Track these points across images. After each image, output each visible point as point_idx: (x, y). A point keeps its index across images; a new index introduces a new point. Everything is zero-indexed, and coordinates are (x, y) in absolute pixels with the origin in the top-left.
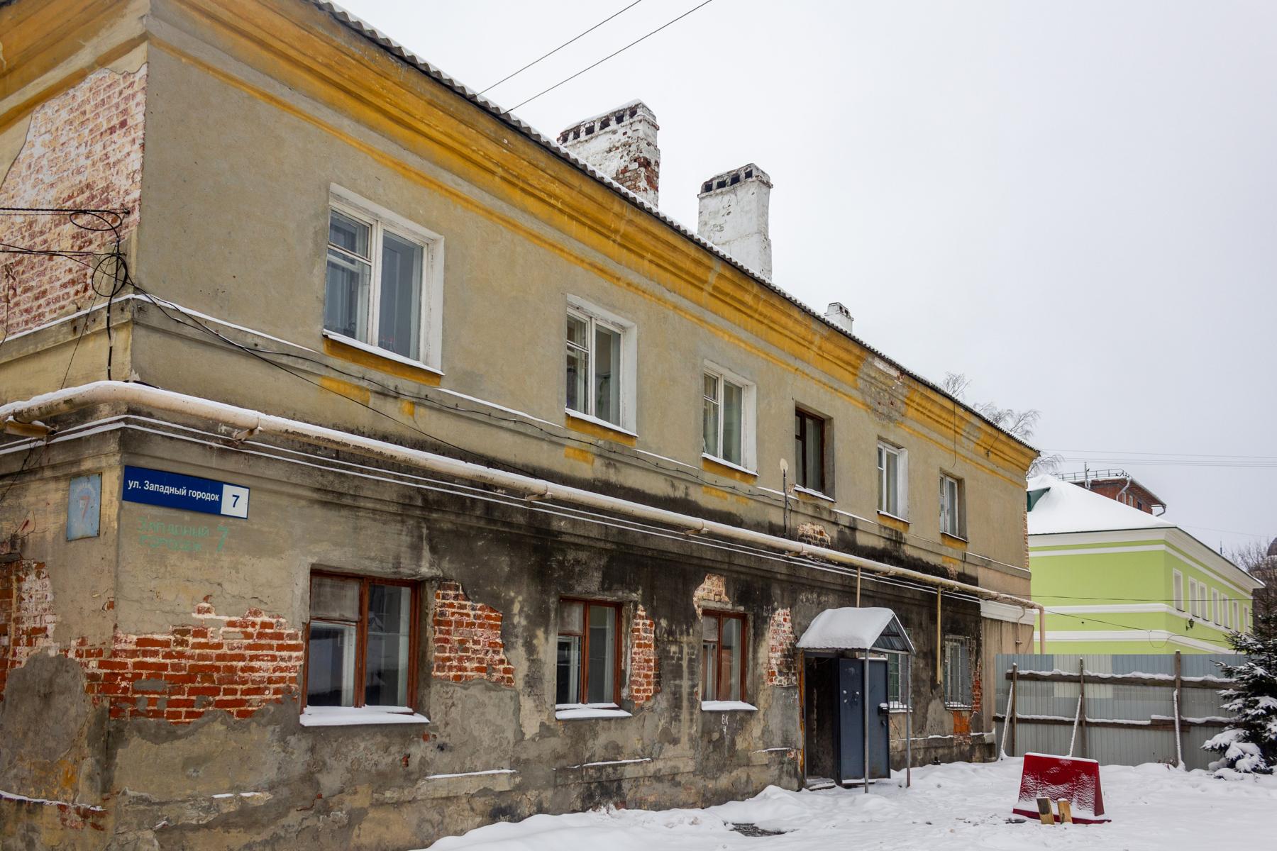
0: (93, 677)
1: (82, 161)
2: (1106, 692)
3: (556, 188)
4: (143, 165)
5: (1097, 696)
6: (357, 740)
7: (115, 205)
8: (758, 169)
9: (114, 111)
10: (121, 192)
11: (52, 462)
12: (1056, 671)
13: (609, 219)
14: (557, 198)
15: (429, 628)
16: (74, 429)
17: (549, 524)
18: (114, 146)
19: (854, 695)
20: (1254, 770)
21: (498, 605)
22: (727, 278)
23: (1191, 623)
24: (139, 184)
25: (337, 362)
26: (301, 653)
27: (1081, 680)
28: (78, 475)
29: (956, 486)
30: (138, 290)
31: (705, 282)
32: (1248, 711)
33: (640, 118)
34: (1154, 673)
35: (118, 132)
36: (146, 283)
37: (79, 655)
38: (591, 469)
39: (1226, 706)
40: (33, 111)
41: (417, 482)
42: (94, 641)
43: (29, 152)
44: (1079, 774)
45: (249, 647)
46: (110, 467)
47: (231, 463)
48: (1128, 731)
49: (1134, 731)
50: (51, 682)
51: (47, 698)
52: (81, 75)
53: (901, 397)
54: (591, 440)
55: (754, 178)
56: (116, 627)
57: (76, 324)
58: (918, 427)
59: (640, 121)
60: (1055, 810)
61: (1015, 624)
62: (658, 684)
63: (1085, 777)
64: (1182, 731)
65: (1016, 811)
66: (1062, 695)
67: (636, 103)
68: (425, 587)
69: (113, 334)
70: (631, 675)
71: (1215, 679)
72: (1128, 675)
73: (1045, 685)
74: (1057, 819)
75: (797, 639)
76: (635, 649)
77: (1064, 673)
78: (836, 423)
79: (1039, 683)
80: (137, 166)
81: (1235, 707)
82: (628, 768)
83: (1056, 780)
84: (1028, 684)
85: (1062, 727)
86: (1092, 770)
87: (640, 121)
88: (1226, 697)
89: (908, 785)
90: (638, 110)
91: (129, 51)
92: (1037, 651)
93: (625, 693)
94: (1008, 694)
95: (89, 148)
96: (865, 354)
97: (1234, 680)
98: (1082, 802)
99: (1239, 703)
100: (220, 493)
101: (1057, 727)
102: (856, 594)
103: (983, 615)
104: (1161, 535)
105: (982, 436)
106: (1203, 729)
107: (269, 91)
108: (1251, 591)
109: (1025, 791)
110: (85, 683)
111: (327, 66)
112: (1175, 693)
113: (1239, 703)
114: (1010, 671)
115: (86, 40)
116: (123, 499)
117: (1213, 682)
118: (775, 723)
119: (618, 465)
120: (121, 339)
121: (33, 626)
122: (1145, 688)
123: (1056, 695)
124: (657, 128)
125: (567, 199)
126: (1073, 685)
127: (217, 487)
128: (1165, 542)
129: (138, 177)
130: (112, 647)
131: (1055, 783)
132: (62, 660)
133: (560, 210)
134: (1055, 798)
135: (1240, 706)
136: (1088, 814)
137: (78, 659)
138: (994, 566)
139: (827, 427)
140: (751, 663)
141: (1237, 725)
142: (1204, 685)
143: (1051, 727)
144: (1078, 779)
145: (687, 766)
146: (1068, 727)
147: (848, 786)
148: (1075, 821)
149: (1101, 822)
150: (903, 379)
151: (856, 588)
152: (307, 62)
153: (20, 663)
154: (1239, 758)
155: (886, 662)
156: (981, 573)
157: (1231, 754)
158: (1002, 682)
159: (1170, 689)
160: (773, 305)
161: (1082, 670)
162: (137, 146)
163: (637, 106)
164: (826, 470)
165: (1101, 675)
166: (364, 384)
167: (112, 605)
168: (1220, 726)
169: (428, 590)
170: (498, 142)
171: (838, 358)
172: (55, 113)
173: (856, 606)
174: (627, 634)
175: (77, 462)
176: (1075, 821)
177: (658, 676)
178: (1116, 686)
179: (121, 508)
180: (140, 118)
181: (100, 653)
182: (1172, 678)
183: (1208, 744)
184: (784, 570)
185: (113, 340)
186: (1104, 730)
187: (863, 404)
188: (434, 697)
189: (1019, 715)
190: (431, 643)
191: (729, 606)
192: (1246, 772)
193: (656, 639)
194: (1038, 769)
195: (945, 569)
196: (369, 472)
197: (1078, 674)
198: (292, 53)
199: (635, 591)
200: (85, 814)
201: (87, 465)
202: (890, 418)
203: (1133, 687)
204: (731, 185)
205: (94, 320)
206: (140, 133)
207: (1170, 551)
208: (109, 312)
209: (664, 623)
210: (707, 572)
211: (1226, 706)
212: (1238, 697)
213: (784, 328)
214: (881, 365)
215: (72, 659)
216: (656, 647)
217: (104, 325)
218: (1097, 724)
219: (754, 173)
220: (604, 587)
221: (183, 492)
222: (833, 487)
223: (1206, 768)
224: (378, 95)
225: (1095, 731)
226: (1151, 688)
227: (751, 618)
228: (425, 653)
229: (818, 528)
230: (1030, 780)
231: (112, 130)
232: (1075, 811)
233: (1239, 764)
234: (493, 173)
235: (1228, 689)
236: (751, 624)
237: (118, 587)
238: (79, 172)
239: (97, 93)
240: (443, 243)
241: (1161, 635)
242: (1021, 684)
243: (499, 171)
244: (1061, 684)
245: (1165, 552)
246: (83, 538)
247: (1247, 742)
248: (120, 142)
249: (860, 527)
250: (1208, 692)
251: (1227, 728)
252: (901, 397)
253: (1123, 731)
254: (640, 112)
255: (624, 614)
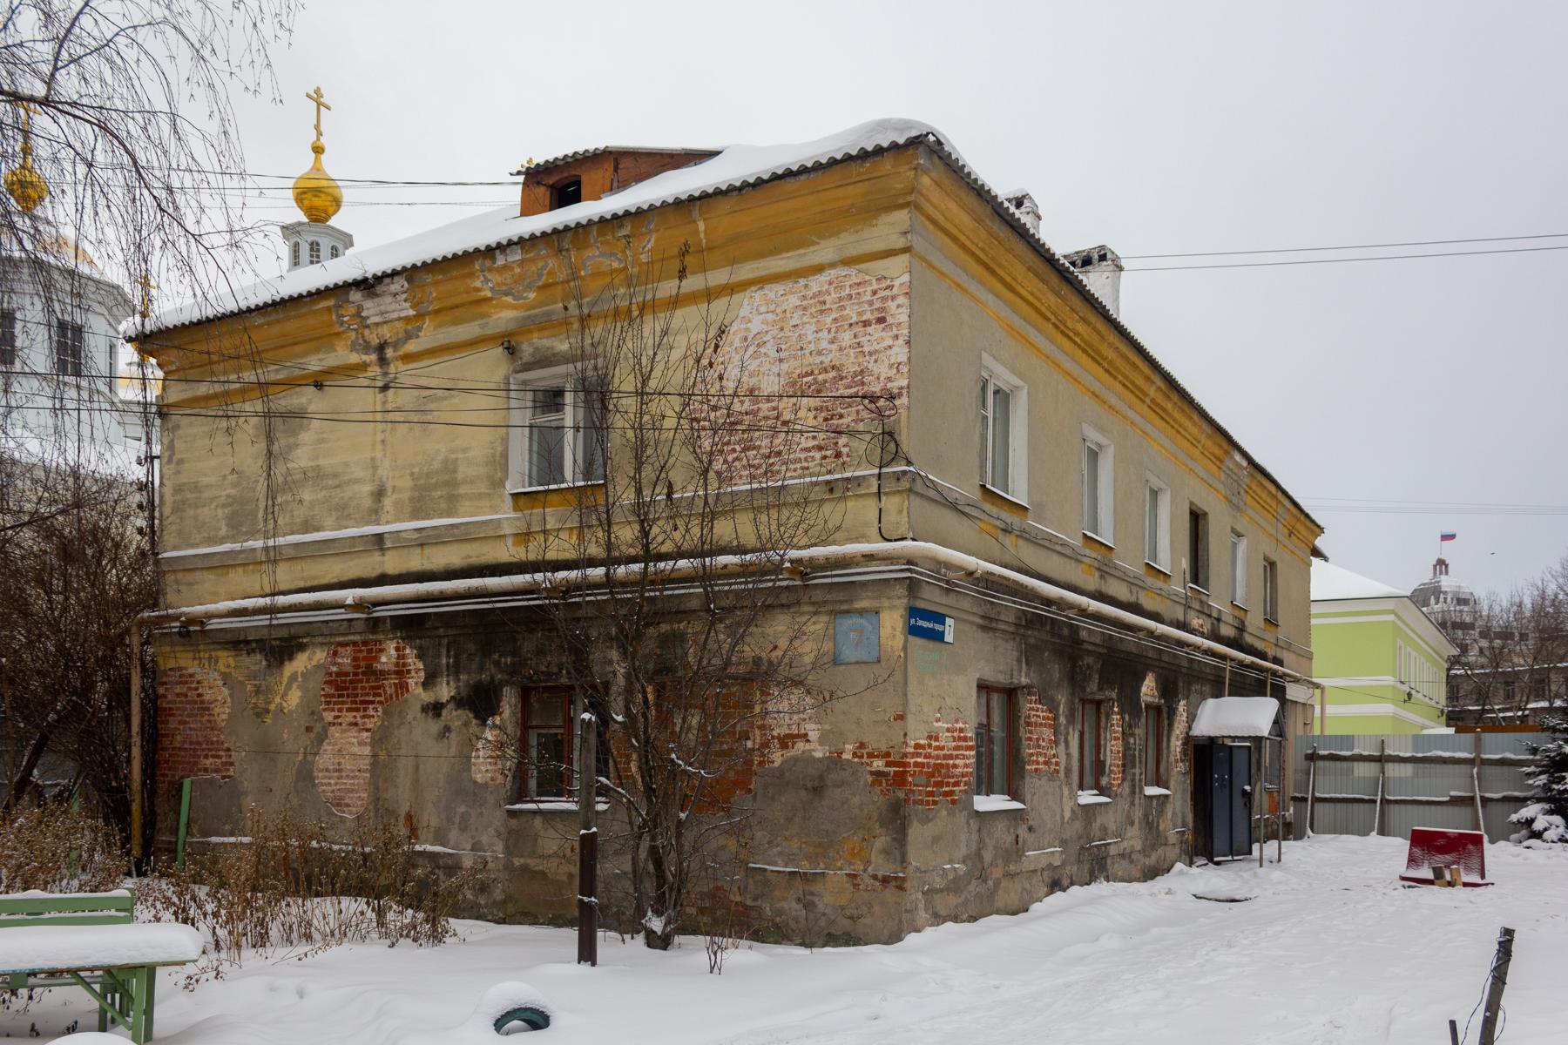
0: (878, 774)
1: (824, 344)
2: (1406, 770)
3: (1080, 327)
4: (909, 359)
5: (1397, 775)
6: (997, 822)
7: (876, 388)
8: (1113, 253)
9: (866, 307)
10: (882, 379)
11: (813, 600)
12: (1356, 751)
13: (1104, 348)
14: (1077, 334)
15: (1022, 729)
16: (834, 573)
17: (1078, 635)
18: (868, 338)
19: (1224, 779)
20: (1560, 840)
21: (1053, 708)
22: (1162, 390)
23: (1410, 695)
24: (906, 375)
25: (987, 507)
26: (973, 753)
27: (1381, 759)
28: (847, 612)
29: (1268, 569)
30: (909, 463)
31: (1146, 395)
32: (1555, 787)
33: (1028, 210)
34: (1454, 752)
35: (873, 326)
36: (913, 458)
37: (855, 755)
38: (1092, 583)
39: (1531, 782)
40: (746, 290)
41: (1021, 604)
42: (876, 742)
43: (743, 326)
44: (1466, 845)
45: (957, 748)
46: (893, 607)
47: (950, 600)
48: (1427, 808)
49: (1433, 808)
50: (821, 778)
51: (818, 790)
52: (819, 269)
53: (1245, 486)
54: (1094, 555)
55: (1110, 262)
56: (905, 735)
57: (832, 485)
58: (1256, 517)
59: (1028, 213)
60: (1448, 877)
61: (1304, 704)
62: (1124, 772)
63: (1471, 847)
64: (1483, 806)
65: (1404, 879)
66: (1362, 775)
67: (1024, 193)
68: (1016, 694)
69: (883, 498)
70: (1110, 766)
71: (1513, 756)
72: (1429, 754)
73: (1345, 764)
74: (1450, 884)
75: (1190, 728)
76: (1113, 742)
77: (1365, 753)
78: (1211, 517)
79: (1338, 763)
80: (903, 358)
81: (1541, 783)
82: (1112, 847)
83: (1443, 850)
84: (1327, 764)
85: (1367, 805)
86: (1477, 841)
87: (1028, 213)
88: (1529, 775)
89: (1279, 860)
90: (1025, 201)
91: (887, 257)
92: (1317, 732)
93: (1104, 781)
94: (1309, 774)
95: (832, 335)
96: (1230, 449)
97: (1538, 757)
98: (1468, 869)
99: (1543, 779)
100: (944, 624)
101: (1356, 806)
102: (1224, 683)
103: (1287, 697)
104: (1390, 605)
105: (1288, 517)
106: (1500, 803)
107: (959, 281)
108: (1446, 657)
109: (1412, 861)
110: (870, 779)
111: (983, 250)
112: (1475, 770)
113: (1543, 779)
114: (1310, 752)
115: (822, 236)
116: (910, 633)
117: (1511, 759)
118: (1178, 809)
119: (1106, 576)
120: (891, 503)
121: (787, 732)
122: (1444, 766)
123: (1356, 774)
124: (1039, 218)
125: (1085, 336)
126: (1373, 764)
127: (940, 619)
128: (1393, 612)
129: (905, 369)
130: (903, 750)
131: (1442, 853)
132: (835, 760)
133: (1079, 346)
134: (1447, 867)
135: (1545, 781)
136: (1476, 879)
137: (856, 760)
138: (1293, 648)
139: (1201, 522)
140: (1165, 751)
141: (1539, 800)
142: (1503, 762)
143: (1350, 805)
144: (1464, 849)
145: (1138, 845)
146: (1303, 804)
147: (1218, 863)
148: (1466, 885)
149: (1487, 884)
150: (1251, 469)
151: (1225, 678)
152: (973, 248)
153: (773, 762)
154: (1546, 829)
155: (1249, 747)
156: (1285, 656)
157: (1538, 826)
158: (1303, 764)
159: (1469, 766)
160: (1183, 411)
161: (1383, 749)
162: (901, 341)
163: (1024, 197)
164: (1200, 564)
165: (1402, 754)
166: (998, 523)
167: (901, 717)
168: (1522, 802)
169: (1020, 695)
170: (1057, 293)
171: (1213, 455)
172: (786, 297)
173: (1266, 696)
174: (1106, 728)
175: (851, 601)
176: (1466, 885)
177: (1124, 765)
178: (1416, 765)
179: (906, 641)
180: (904, 318)
181: (887, 755)
182: (1472, 756)
183: (1514, 817)
184: (1185, 664)
185: (883, 502)
186: (1403, 807)
187: (1224, 497)
188: (1032, 785)
189: (1317, 795)
190: (1024, 741)
191: (1157, 700)
192: (1553, 842)
193: (1123, 733)
194: (1424, 843)
195: (1266, 653)
196: (999, 598)
197: (1378, 754)
198: (963, 238)
199: (1113, 690)
200: (885, 880)
201: (863, 604)
202: (1238, 508)
203: (1433, 765)
204: (1082, 267)
205: (859, 485)
206: (906, 331)
207: (1399, 623)
208: (879, 479)
209: (1127, 717)
210: (1148, 669)
211: (1531, 782)
212: (1541, 773)
213: (1186, 430)
214: (1238, 457)
215: (847, 760)
216: (1123, 739)
217: (875, 489)
218: (1396, 802)
219: (1109, 256)
220: (1100, 689)
221: (931, 626)
222: (1207, 579)
223: (1508, 840)
224: (1000, 265)
225: (1394, 809)
226: (1451, 766)
227: (1165, 710)
228: (1018, 750)
229: (1201, 622)
230: (1417, 851)
231: (866, 324)
232: (1466, 878)
233: (1546, 835)
234: (1048, 319)
235: (1529, 767)
236: (1165, 715)
237: (905, 704)
238: (820, 353)
239: (842, 288)
240: (1026, 391)
241: (1387, 708)
242: (1320, 764)
243: (1052, 318)
244: (1361, 764)
245: (1393, 622)
246: (857, 663)
247: (1552, 814)
248: (876, 335)
249: (1223, 619)
250: (1506, 769)
251: (1529, 802)
252: (1245, 486)
253: (1421, 807)
254: (1027, 203)
255: (1102, 711)
